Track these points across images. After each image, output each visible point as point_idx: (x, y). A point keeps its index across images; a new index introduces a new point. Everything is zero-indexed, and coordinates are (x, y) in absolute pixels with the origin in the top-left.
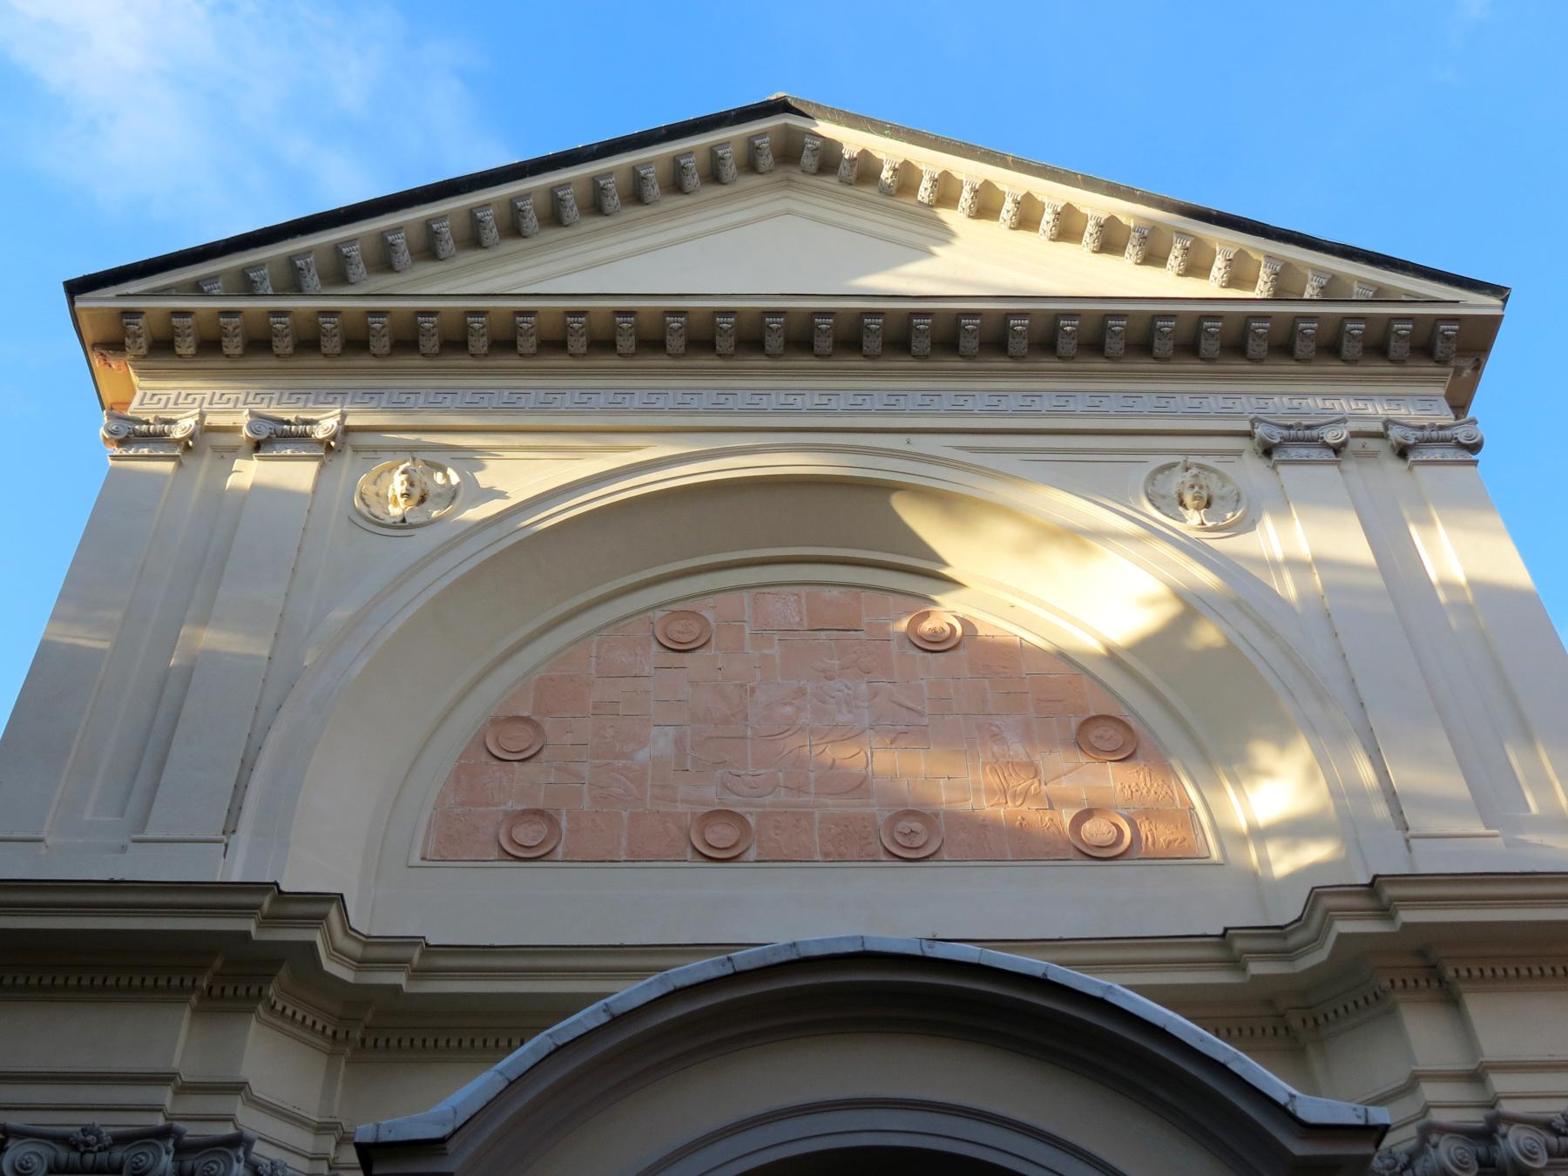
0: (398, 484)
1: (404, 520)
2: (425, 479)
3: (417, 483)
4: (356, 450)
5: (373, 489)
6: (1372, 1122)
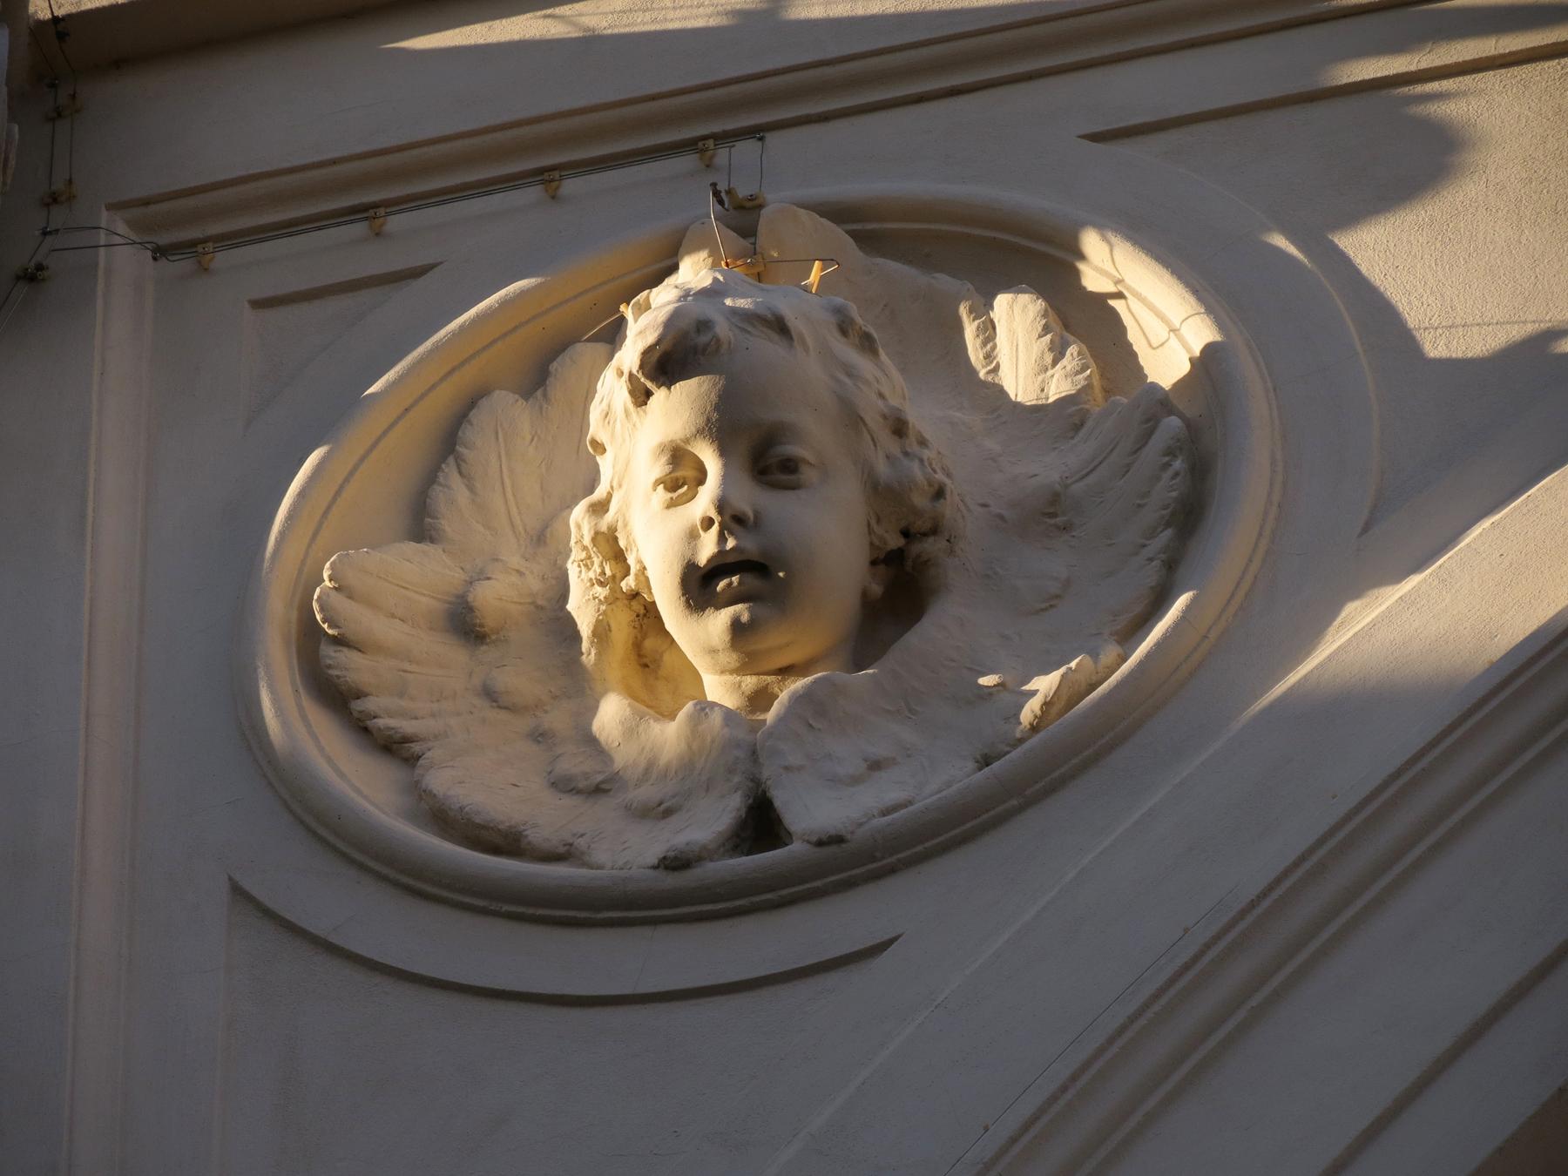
0: (638, 481)
1: (761, 824)
2: (885, 382)
3: (815, 438)
4: (186, 236)
5: (421, 573)
6: (59, 13)
